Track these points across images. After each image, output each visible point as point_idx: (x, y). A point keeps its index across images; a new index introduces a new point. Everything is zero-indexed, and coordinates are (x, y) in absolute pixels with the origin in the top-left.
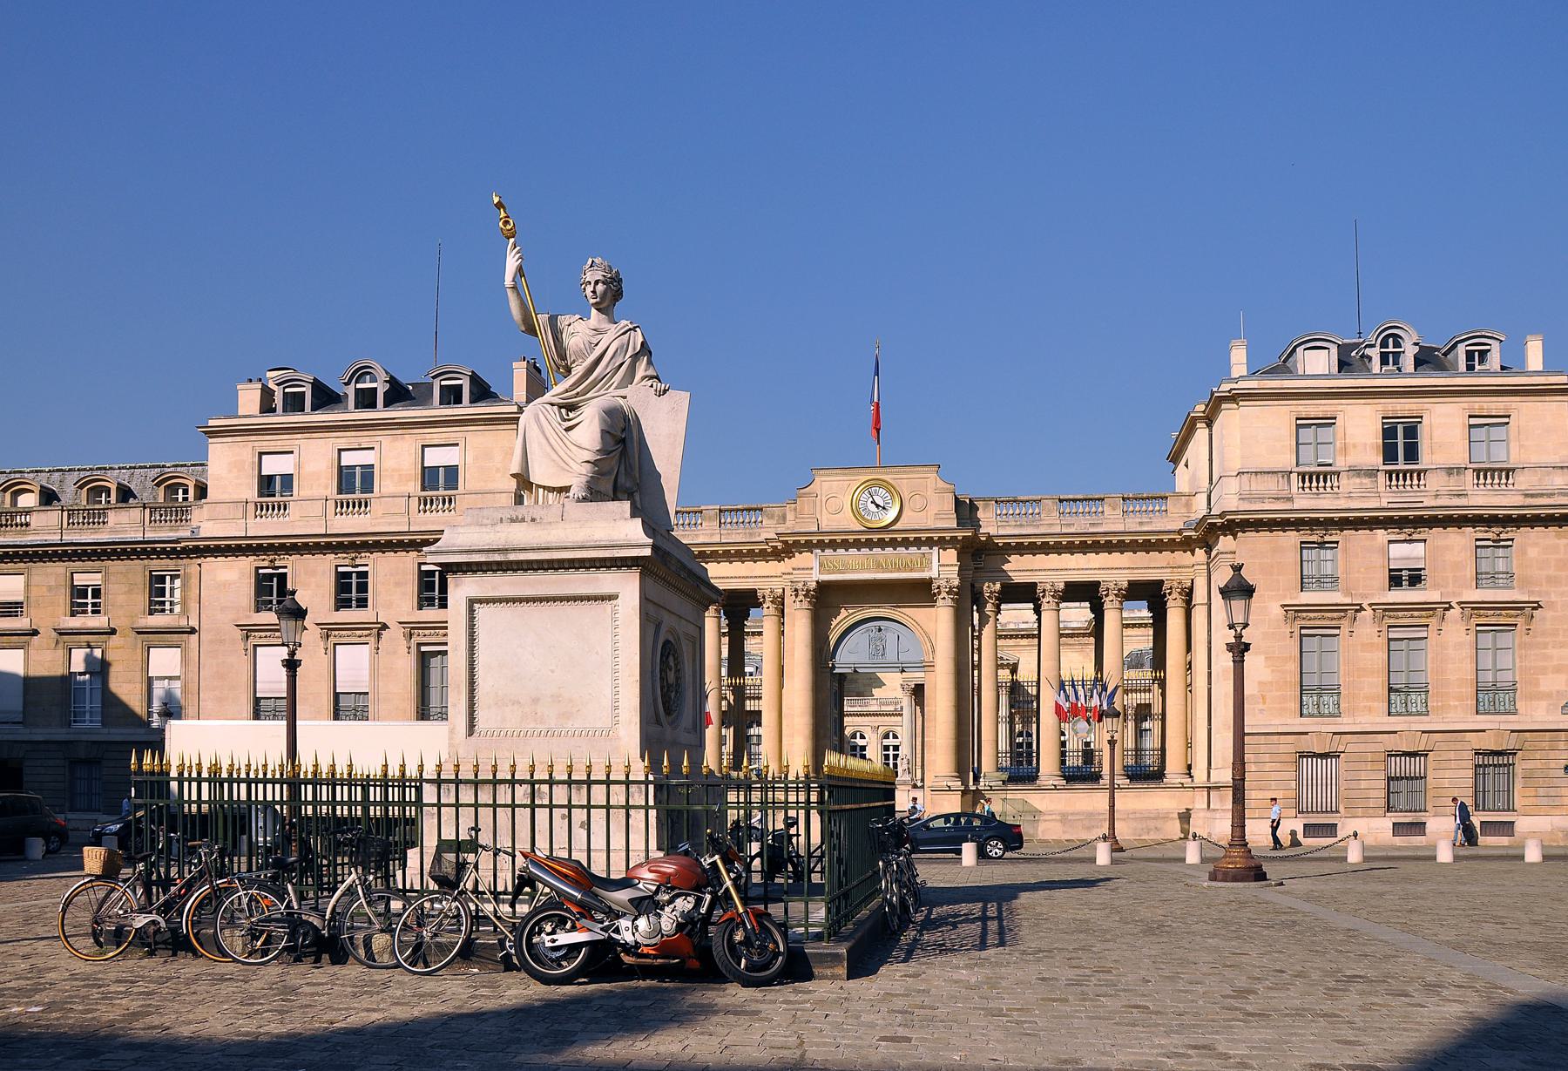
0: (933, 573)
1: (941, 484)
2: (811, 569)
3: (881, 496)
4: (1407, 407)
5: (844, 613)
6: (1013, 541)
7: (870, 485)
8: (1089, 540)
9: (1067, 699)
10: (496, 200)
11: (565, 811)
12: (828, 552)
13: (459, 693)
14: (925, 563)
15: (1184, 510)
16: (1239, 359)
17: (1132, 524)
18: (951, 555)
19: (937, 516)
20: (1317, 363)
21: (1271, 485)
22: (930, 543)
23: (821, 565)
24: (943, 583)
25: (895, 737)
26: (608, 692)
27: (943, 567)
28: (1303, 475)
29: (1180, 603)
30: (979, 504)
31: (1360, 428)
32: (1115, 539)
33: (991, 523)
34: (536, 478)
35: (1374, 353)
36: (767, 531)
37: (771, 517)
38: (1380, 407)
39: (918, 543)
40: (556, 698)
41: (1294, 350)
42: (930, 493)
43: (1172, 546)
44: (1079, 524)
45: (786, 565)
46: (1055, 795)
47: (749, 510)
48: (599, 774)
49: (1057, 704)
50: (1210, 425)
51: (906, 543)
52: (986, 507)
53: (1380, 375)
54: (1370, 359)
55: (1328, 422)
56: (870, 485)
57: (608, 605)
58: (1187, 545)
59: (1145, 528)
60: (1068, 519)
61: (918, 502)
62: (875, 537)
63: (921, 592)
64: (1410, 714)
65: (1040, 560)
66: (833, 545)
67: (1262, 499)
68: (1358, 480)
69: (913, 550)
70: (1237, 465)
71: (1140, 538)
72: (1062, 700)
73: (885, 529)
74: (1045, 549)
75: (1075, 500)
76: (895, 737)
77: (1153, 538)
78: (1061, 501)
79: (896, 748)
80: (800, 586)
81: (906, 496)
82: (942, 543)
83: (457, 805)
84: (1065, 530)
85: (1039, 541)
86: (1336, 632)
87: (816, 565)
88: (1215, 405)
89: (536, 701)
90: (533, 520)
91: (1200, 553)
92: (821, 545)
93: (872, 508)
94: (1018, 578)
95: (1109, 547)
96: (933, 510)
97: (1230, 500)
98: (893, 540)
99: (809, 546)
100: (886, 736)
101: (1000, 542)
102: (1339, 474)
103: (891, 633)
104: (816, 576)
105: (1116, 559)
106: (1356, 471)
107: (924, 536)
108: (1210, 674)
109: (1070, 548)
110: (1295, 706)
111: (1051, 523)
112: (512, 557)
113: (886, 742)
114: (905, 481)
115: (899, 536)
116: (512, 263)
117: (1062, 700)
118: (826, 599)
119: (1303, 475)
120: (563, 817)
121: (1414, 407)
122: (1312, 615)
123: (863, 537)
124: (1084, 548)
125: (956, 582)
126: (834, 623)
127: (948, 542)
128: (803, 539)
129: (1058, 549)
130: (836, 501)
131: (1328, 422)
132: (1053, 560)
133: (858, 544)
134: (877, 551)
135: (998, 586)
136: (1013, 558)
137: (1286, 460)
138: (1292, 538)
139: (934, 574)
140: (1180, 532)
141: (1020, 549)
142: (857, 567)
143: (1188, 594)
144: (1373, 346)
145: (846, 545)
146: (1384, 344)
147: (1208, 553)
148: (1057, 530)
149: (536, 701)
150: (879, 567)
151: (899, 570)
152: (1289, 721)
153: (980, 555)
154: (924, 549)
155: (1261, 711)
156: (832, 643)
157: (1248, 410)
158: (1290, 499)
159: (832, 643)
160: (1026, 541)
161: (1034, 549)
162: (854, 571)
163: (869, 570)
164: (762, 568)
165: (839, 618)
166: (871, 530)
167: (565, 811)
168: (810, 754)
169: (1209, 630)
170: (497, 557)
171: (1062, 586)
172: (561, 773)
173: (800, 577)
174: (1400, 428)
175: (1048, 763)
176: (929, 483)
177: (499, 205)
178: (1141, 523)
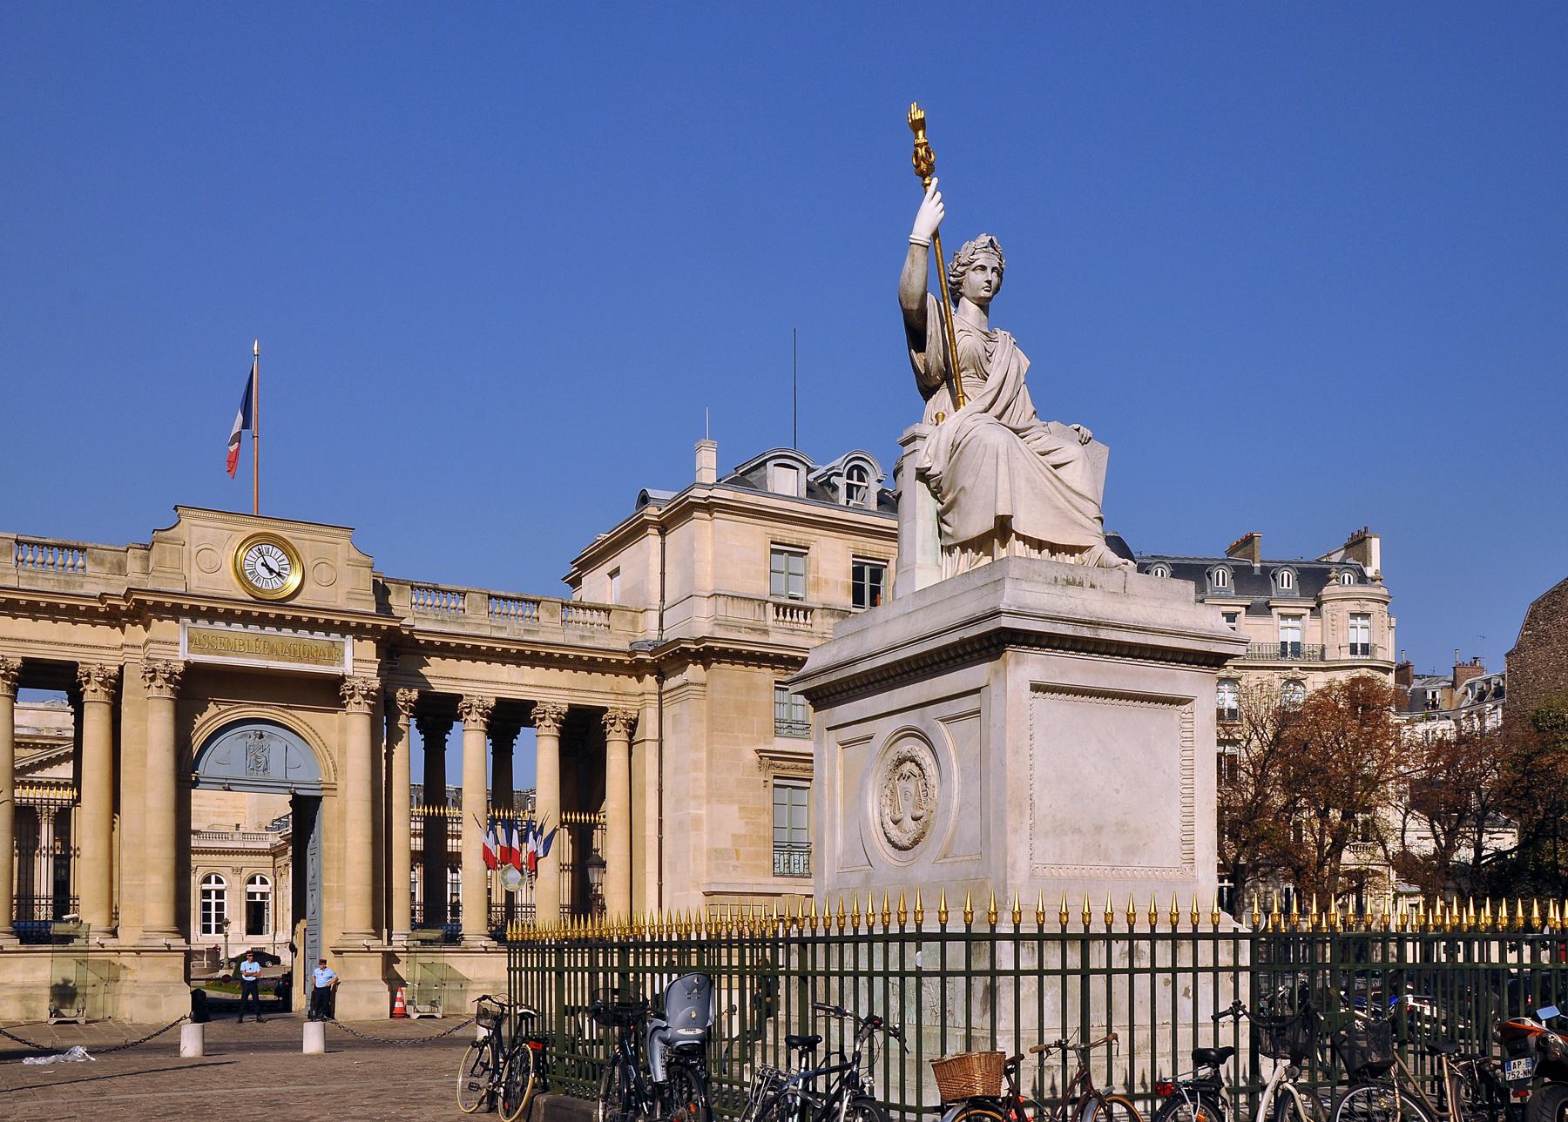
0: (346, 667)
1: (355, 555)
2: (177, 645)
3: (275, 558)
4: (876, 548)
5: (212, 709)
6: (438, 640)
7: (253, 541)
8: (528, 650)
9: (497, 842)
10: (919, 115)
11: (1169, 976)
12: (202, 624)
13: (1021, 814)
14: (335, 655)
15: (629, 628)
16: (707, 464)
17: (570, 637)
18: (369, 648)
19: (350, 595)
20: (785, 483)
21: (746, 613)
22: (344, 629)
23: (190, 641)
24: (358, 683)
25: (219, 881)
26: (1176, 823)
27: (357, 662)
28: (777, 606)
29: (101, 695)
30: (392, 587)
31: (832, 561)
32: (557, 652)
33: (411, 613)
34: (1019, 526)
35: (841, 483)
36: (95, 582)
37: (101, 563)
38: (850, 544)
39: (328, 627)
40: (1121, 827)
41: (764, 463)
42: (340, 563)
43: (617, 668)
44: (512, 628)
45: (136, 633)
46: (485, 958)
47: (61, 547)
48: (1005, 928)
49: (485, 847)
50: (663, 534)
51: (312, 625)
52: (399, 592)
53: (846, 508)
54: (835, 488)
55: (800, 551)
56: (253, 541)
57: (1187, 707)
58: (636, 669)
59: (587, 644)
60: (499, 621)
61: (326, 574)
62: (273, 612)
63: (326, 692)
64: (792, 875)
65: (466, 668)
66: (212, 615)
67: (738, 628)
68: (832, 621)
69: (320, 635)
70: (708, 586)
71: (586, 655)
72: (490, 844)
73: (280, 603)
74: (474, 654)
75: (505, 599)
76: (219, 881)
77: (600, 656)
78: (490, 597)
79: (220, 894)
80: (160, 665)
81: (309, 562)
82: (359, 632)
83: (1041, 972)
84: (495, 634)
85: (469, 643)
86: (807, 784)
87: (183, 639)
88: (683, 512)
89: (1099, 829)
90: (1092, 586)
91: (650, 681)
92: (195, 613)
93: (264, 572)
94: (440, 687)
95: (549, 661)
96: (344, 586)
97: (700, 623)
98: (280, 617)
99: (176, 612)
100: (252, 881)
101: (422, 638)
102: (812, 610)
103: (277, 742)
104: (182, 655)
105: (554, 676)
106: (829, 610)
107: (338, 619)
108: (660, 822)
109: (504, 657)
110: (768, 863)
111: (478, 622)
112: (1104, 634)
113: (251, 888)
114: (304, 540)
115: (305, 616)
116: (930, 213)
117: (490, 844)
118: (194, 687)
119: (777, 606)
120: (1166, 983)
121: (882, 549)
122: (786, 764)
123: (256, 611)
124: (520, 659)
125: (376, 684)
126: (199, 721)
127: (367, 631)
128: (168, 601)
129: (490, 656)
130: (209, 555)
131: (800, 551)
132: (480, 669)
133: (246, 619)
134: (270, 630)
135: (415, 695)
136: (433, 661)
137: (760, 588)
138: (766, 676)
139: (349, 672)
140: (631, 654)
141: (445, 651)
142: (244, 650)
143: (632, 725)
144: (840, 475)
145: (229, 617)
146: (850, 477)
147: (660, 682)
148: (486, 632)
149: (1099, 829)
150: (273, 652)
151: (300, 660)
152: (763, 880)
153: (400, 652)
154: (335, 637)
155: (735, 867)
156: (195, 749)
157: (723, 522)
158: (766, 632)
159: (195, 749)
160: (453, 641)
161: (460, 653)
162: (238, 653)
163: (258, 654)
164: (84, 633)
165: (206, 715)
166: (260, 601)
167: (1169, 976)
168: (171, 899)
169: (660, 772)
170: (1086, 632)
171: (492, 703)
172: (980, 922)
173: (160, 653)
174: (867, 569)
175: (472, 921)
176: (341, 547)
177: (920, 124)
178: (582, 637)
